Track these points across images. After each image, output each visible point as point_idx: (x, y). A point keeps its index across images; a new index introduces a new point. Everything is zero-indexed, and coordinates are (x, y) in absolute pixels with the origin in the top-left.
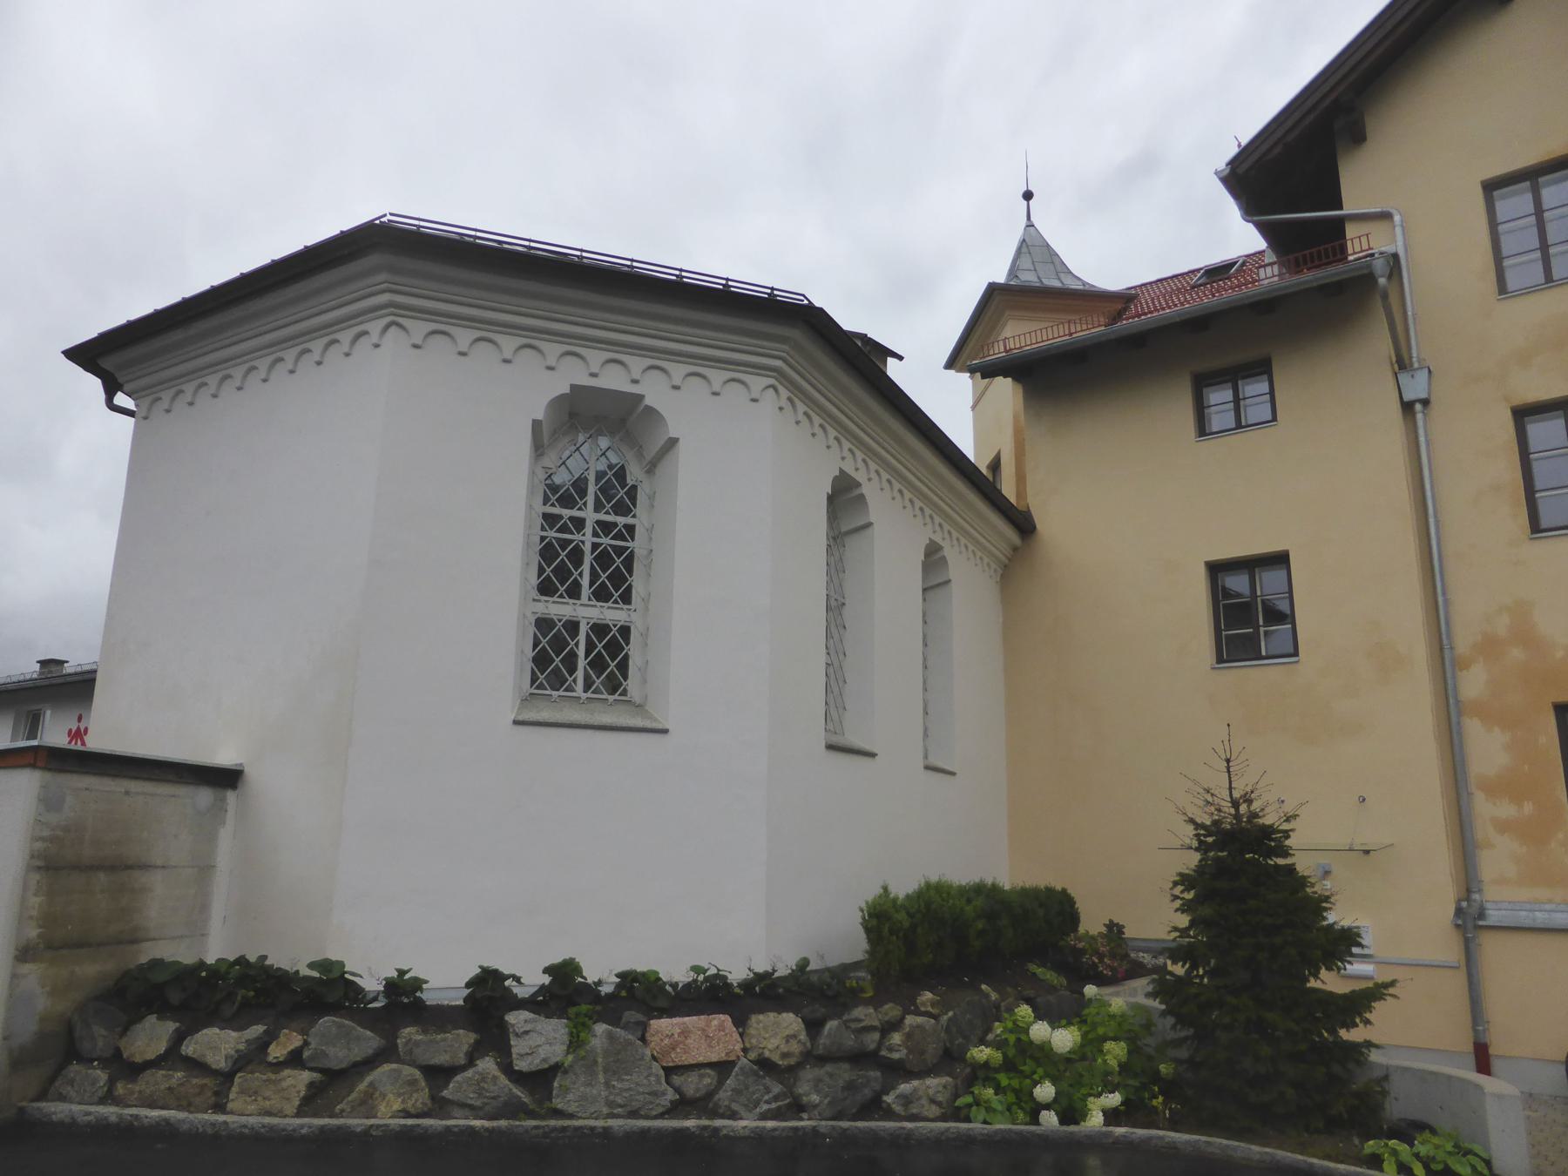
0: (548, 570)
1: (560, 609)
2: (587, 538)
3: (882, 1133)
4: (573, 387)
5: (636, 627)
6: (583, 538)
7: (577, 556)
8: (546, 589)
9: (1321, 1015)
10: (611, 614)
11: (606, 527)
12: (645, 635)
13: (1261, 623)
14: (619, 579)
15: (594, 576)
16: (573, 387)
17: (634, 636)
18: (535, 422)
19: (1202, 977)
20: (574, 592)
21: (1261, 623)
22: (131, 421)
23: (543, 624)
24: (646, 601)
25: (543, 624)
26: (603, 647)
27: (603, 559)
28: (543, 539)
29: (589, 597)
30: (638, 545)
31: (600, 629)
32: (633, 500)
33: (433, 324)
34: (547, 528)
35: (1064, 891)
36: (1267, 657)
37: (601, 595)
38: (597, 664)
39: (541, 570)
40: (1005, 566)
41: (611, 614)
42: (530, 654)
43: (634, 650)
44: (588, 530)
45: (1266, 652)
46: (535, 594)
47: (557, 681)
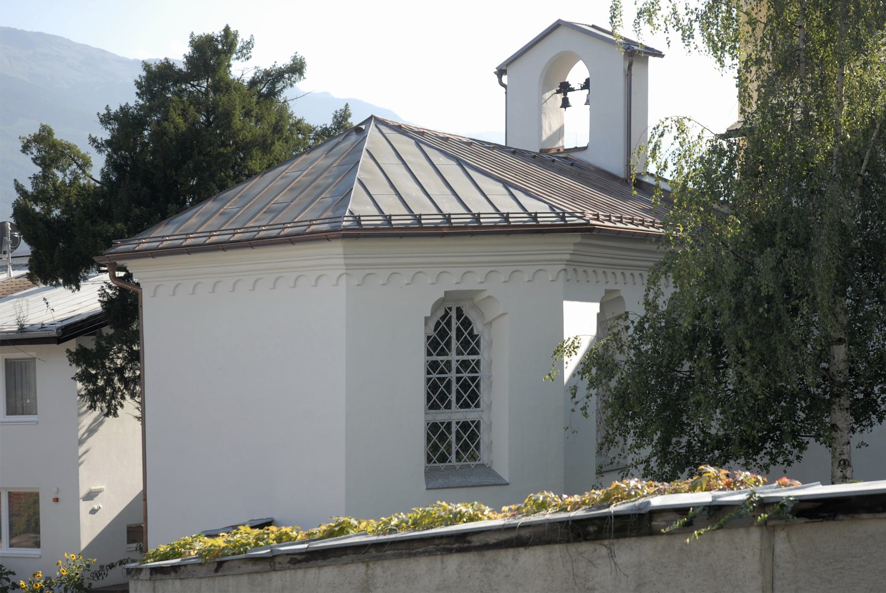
0: (434, 397)
1: (441, 416)
2: (453, 375)
3: (391, 123)
4: (446, 293)
5: (484, 421)
6: (451, 376)
7: (448, 386)
9: (764, 91)
10: (469, 415)
11: (465, 364)
12: (490, 426)
14: (474, 396)
16: (446, 293)
17: (482, 427)
19: (707, 458)
20: (448, 407)
24: (490, 406)
26: (444, 387)
27: (465, 386)
28: (429, 380)
29: (428, 351)
30: (482, 374)
31: (465, 426)
32: (478, 346)
34: (432, 372)
37: (465, 405)
43: (484, 437)
44: (454, 365)
47: (443, 459)
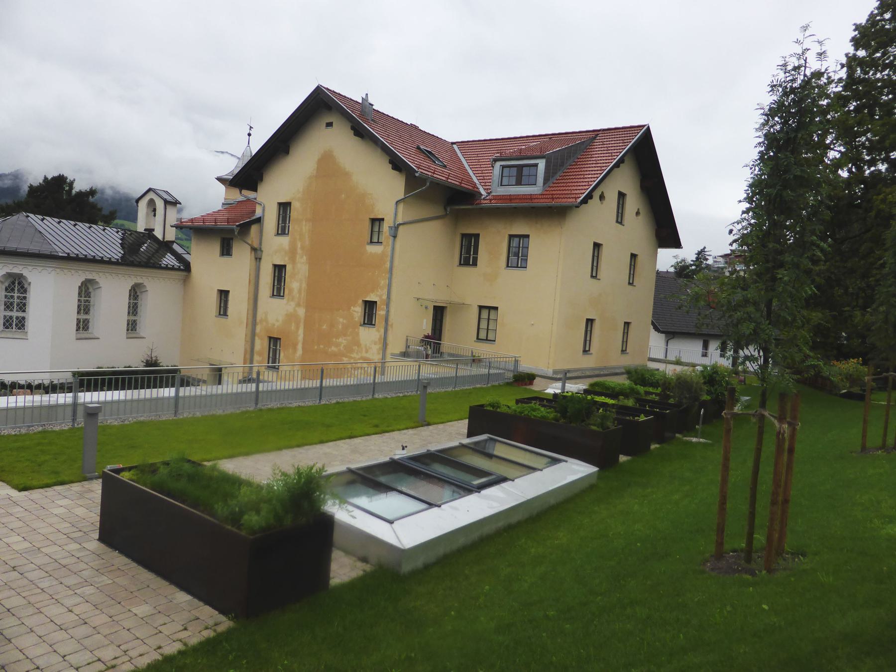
8: (24, 318)
10: (9, 313)
13: (472, 254)
15: (13, 321)
18: (659, 369)
21: (472, 254)
22: (652, 356)
23: (24, 311)
25: (24, 311)
33: (590, 379)
35: (190, 263)
36: (510, 267)
37: (11, 317)
38: (84, 310)
39: (25, 322)
40: (425, 387)
41: (9, 313)
42: (26, 306)
45: (521, 265)
46: (26, 317)
